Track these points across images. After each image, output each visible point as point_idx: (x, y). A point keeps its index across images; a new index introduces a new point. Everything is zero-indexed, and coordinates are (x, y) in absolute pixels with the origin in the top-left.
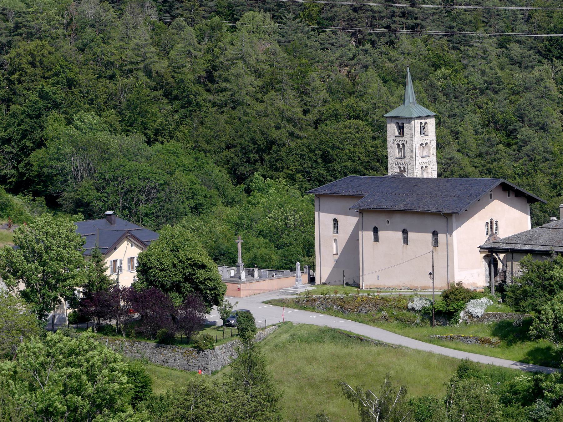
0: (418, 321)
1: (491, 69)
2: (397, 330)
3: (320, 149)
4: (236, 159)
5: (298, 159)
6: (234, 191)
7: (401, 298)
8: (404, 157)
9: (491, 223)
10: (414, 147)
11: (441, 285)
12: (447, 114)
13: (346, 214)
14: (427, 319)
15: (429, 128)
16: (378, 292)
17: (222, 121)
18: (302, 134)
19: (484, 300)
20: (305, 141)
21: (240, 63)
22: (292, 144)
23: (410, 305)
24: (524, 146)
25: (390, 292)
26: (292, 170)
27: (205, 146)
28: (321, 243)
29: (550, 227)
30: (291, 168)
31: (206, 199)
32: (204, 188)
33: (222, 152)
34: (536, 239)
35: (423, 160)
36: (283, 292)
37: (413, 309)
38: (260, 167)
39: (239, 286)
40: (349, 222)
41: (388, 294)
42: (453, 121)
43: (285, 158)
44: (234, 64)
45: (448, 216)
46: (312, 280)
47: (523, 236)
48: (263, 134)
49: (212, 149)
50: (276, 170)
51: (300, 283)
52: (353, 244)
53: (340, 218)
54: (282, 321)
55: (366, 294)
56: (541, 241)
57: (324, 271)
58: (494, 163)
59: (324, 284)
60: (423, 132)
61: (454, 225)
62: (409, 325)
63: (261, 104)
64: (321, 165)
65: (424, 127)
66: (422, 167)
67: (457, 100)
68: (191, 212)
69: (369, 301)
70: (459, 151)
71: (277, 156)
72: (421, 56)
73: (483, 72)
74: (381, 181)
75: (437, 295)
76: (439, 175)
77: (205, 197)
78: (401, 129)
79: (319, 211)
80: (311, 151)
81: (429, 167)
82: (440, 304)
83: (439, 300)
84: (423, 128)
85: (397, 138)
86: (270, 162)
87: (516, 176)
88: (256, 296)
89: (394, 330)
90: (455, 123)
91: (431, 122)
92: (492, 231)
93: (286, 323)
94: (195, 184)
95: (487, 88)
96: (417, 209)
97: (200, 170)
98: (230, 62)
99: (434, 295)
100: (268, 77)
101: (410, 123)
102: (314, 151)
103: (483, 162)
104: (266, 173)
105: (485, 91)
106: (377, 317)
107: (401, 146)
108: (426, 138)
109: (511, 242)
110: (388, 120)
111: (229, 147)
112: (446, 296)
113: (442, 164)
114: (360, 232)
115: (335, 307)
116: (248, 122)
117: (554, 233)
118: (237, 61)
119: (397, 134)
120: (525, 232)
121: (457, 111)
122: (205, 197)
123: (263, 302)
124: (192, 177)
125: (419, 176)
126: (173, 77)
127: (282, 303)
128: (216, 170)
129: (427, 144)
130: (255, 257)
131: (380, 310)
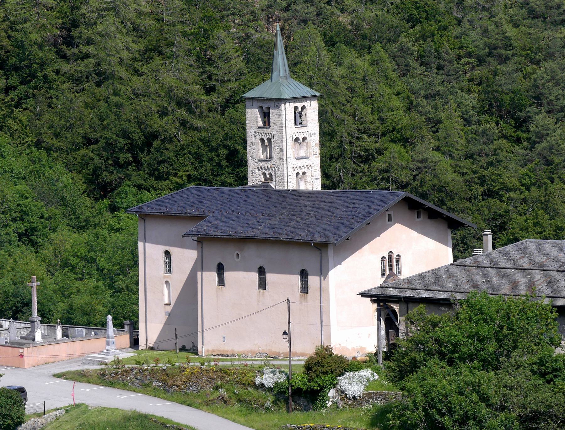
0: (268, 404)
1: (497, 25)
2: (238, 418)
3: (226, 147)
4: (97, 161)
5: (193, 160)
6: (86, 206)
7: (247, 370)
8: (271, 158)
9: (390, 257)
10: (284, 143)
11: (305, 348)
12: (422, 93)
13: (182, 246)
14: (282, 401)
15: (308, 116)
16: (215, 360)
17: (79, 103)
18: (198, 123)
19: (366, 373)
20: (204, 134)
21: (111, 18)
22: (183, 139)
23: (258, 381)
24: (538, 143)
25: (231, 360)
26: (181, 177)
27: (55, 143)
28: (147, 286)
29: (466, 264)
30: (180, 174)
31: (43, 220)
32: (40, 204)
33: (79, 149)
34: (444, 282)
35: (299, 163)
36: (87, 360)
37: (263, 385)
38: (135, 173)
39: (21, 350)
40: (186, 257)
41: (229, 363)
42: (433, 103)
43: (174, 159)
44: (102, 16)
45: (321, 247)
46: (135, 343)
47: (425, 277)
48: (139, 123)
49: (63, 145)
50: (159, 178)
51: (113, 347)
52: (190, 290)
53: (175, 251)
54: (72, 403)
55: (198, 364)
56: (451, 285)
57: (151, 329)
58: (491, 169)
59: (152, 349)
60: (299, 121)
61: (331, 261)
62: (256, 410)
63: (141, 79)
64: (228, 170)
65: (300, 113)
66: (297, 174)
67: (441, 72)
68: (19, 240)
69: (201, 374)
70: (437, 149)
71: (160, 156)
72: (391, 7)
73: (485, 32)
74: (233, 194)
75: (297, 366)
76: (324, 186)
77: (42, 217)
78: (266, 116)
79: (145, 240)
80: (212, 149)
81: (308, 173)
82: (299, 378)
83: (299, 373)
84: (299, 116)
85: (260, 131)
86: (150, 165)
87: (523, 188)
88: (48, 366)
89: (233, 416)
90: (435, 108)
91: (312, 109)
92: (391, 269)
93: (78, 406)
94: (27, 198)
95: (490, 55)
96: (278, 236)
97: (39, 177)
98: (96, 15)
99: (290, 366)
100: (153, 36)
101: (278, 107)
102: (217, 150)
103: (474, 166)
104: (142, 182)
105: (488, 59)
106: (211, 398)
107: (266, 141)
108: (304, 129)
109: (406, 286)
110: (248, 103)
111: (88, 142)
112: (308, 368)
113: (410, 169)
114: (199, 274)
115: (154, 383)
116: (118, 105)
117: (470, 274)
118: (107, 13)
119: (261, 124)
120: (428, 272)
121: (440, 88)
122: (42, 217)
123: (54, 376)
124: (23, 187)
125: (292, 186)
126: (9, 37)
127: (80, 377)
128: (66, 178)
129: (304, 139)
130: (71, 309)
131: (217, 388)
